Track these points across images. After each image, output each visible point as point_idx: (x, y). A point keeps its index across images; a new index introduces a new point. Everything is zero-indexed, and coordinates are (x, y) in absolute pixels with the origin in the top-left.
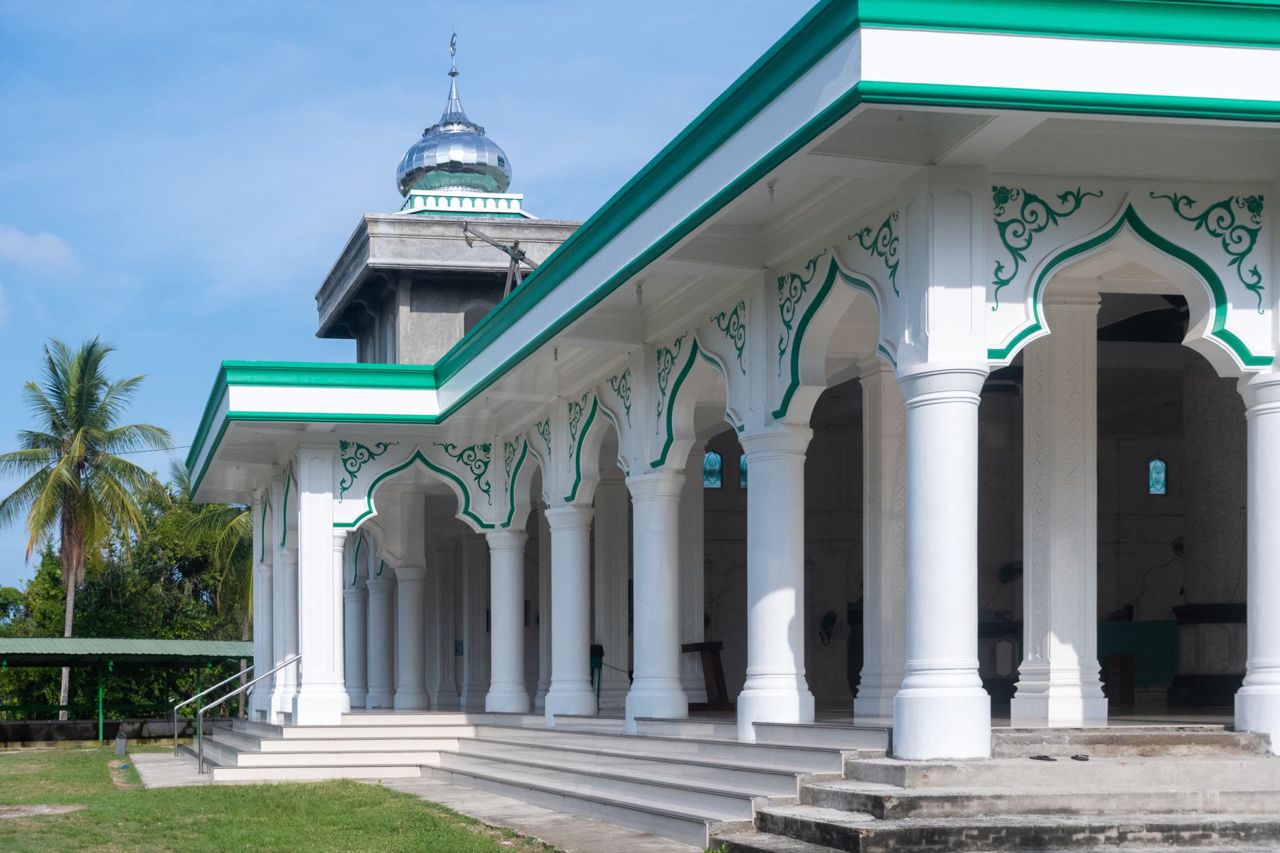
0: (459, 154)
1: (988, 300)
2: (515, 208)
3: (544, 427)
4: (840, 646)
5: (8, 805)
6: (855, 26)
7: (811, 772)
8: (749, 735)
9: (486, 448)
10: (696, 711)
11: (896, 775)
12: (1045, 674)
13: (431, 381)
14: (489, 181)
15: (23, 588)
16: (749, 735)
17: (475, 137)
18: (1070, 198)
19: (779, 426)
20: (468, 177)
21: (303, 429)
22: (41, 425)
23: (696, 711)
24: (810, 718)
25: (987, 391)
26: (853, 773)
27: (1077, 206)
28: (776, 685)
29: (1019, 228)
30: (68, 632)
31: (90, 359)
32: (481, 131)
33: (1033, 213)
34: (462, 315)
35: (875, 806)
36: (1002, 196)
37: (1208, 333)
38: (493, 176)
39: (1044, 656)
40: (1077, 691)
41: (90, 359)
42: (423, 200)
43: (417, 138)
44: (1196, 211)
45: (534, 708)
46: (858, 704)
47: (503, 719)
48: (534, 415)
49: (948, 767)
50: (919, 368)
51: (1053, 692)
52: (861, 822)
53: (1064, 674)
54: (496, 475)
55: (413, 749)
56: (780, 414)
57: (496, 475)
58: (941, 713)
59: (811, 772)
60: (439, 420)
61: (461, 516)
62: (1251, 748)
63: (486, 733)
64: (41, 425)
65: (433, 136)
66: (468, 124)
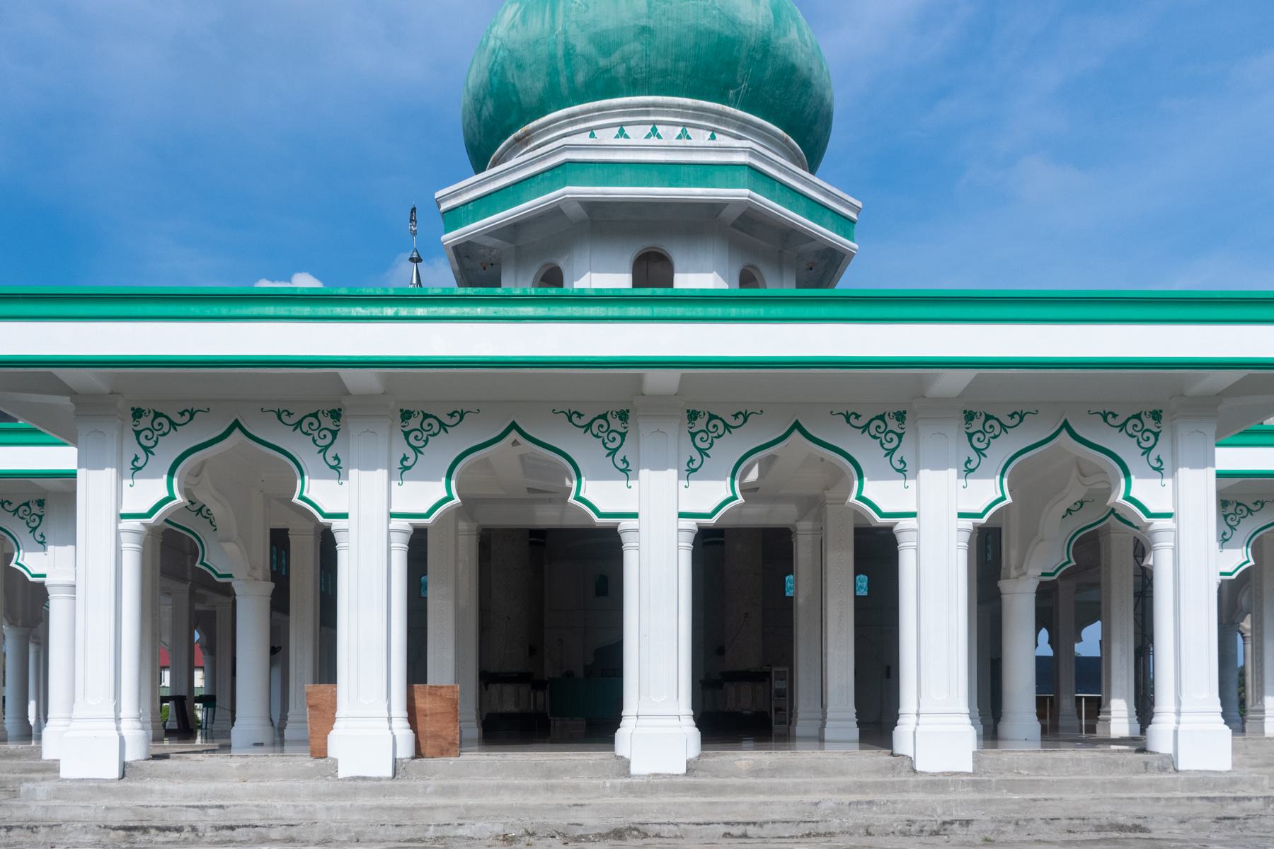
1: (959, 477)
5: (99, 787)
18: (741, 416)
27: (745, 421)
29: (149, 434)
33: (991, 426)
37: (1120, 499)
40: (1126, 721)
44: (1119, 421)
51: (1266, 720)
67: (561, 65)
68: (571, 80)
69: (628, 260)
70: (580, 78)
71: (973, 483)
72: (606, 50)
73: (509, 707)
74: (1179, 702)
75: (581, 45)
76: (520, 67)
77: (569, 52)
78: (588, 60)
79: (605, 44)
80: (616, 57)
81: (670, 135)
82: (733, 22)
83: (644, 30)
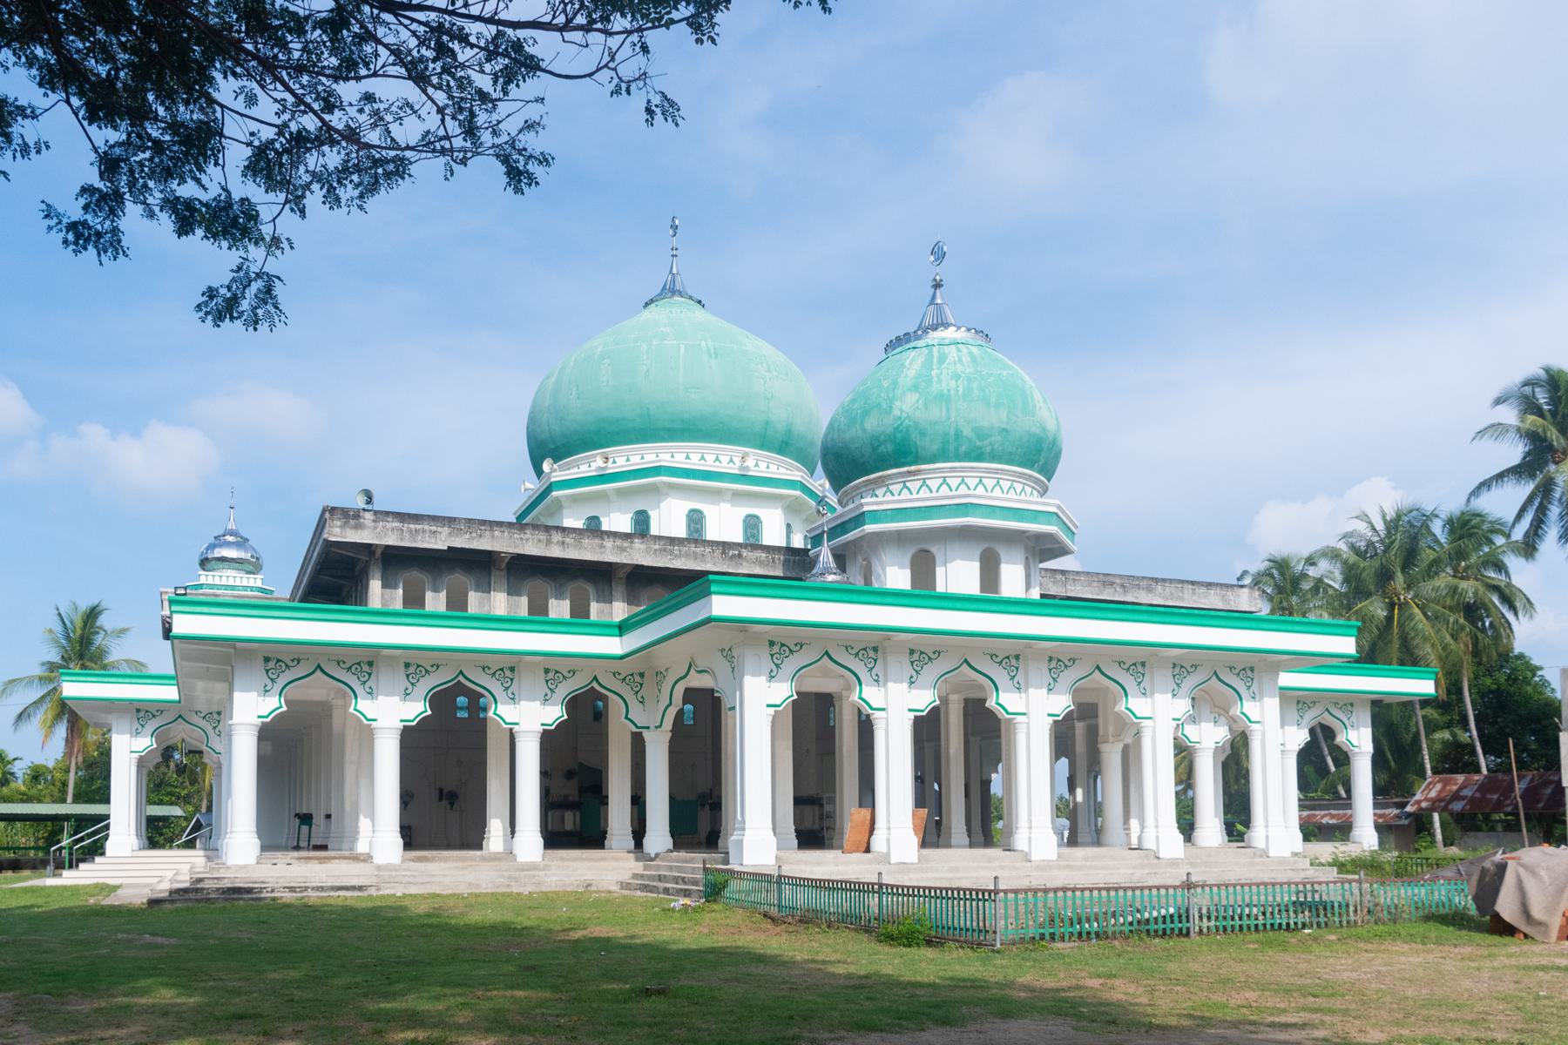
2: (259, 583)
13: (616, 631)
14: (251, 568)
15: (51, 765)
17: (242, 543)
21: (745, 630)
22: (54, 656)
30: (69, 799)
31: (93, 614)
37: (856, 698)
41: (93, 614)
60: (622, 657)
64: (54, 656)
65: (219, 542)
67: (951, 439)
68: (957, 449)
69: (978, 554)
70: (963, 449)
71: (1052, 697)
72: (982, 438)
73: (569, 826)
74: (1030, 821)
75: (967, 432)
76: (923, 434)
77: (958, 435)
78: (970, 440)
79: (981, 434)
80: (986, 442)
81: (773, 468)
82: (1044, 429)
83: (1004, 430)
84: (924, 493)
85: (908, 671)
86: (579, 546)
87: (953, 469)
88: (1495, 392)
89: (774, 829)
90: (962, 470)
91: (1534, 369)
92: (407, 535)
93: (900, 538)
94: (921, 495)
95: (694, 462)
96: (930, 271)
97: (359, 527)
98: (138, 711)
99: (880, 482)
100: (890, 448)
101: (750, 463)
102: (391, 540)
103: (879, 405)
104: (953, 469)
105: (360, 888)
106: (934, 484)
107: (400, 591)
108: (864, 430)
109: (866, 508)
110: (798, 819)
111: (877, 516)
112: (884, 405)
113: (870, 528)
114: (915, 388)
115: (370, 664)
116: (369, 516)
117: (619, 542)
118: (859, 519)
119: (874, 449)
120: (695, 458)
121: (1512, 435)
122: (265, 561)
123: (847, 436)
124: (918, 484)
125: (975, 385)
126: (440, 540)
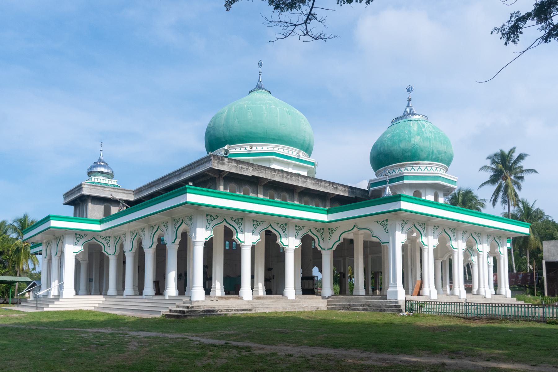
0: (102, 169)
2: (116, 183)
3: (124, 235)
4: (183, 281)
6: (186, 193)
7: (178, 303)
8: (167, 298)
9: (109, 237)
10: (156, 294)
11: (191, 303)
12: (215, 288)
14: (110, 176)
16: (167, 298)
17: (106, 165)
19: (173, 245)
20: (105, 175)
23: (156, 294)
24: (178, 295)
25: (205, 244)
26: (184, 303)
28: (172, 289)
32: (107, 164)
34: (103, 206)
35: (188, 307)
36: (207, 215)
38: (110, 176)
39: (215, 284)
42: (94, 179)
43: (92, 164)
45: (141, 294)
46: (186, 293)
47: (111, 296)
48: (122, 232)
49: (198, 302)
50: (195, 240)
52: (186, 310)
53: (218, 287)
54: (112, 243)
55: (92, 303)
56: (174, 242)
57: (112, 243)
58: (197, 293)
59: (178, 303)
60: (100, 231)
61: (103, 251)
62: (240, 299)
63: (108, 299)
65: (96, 165)
66: (104, 163)
70: (434, 157)
71: (76, 247)
72: (439, 154)
75: (435, 151)
76: (422, 151)
77: (433, 152)
79: (439, 152)
84: (426, 171)
85: (295, 233)
86: (292, 179)
87: (429, 164)
88: (487, 156)
89: (404, 287)
90: (432, 164)
91: (497, 151)
92: (239, 169)
93: (411, 186)
94: (419, 171)
95: (285, 153)
96: (408, 95)
97: (223, 164)
98: (76, 234)
99: (403, 166)
100: (409, 154)
101: (301, 154)
102: (233, 171)
103: (405, 139)
104: (429, 164)
105: (250, 310)
106: (423, 168)
107: (347, 195)
108: (400, 147)
109: (404, 175)
110: (303, 284)
111: (408, 178)
112: (408, 139)
113: (406, 181)
114: (418, 134)
115: (242, 219)
116: (226, 160)
117: (303, 179)
118: (401, 178)
119: (403, 154)
120: (286, 151)
121: (490, 170)
122: (115, 174)
123: (392, 149)
124: (418, 168)
125: (437, 136)
126: (249, 172)
